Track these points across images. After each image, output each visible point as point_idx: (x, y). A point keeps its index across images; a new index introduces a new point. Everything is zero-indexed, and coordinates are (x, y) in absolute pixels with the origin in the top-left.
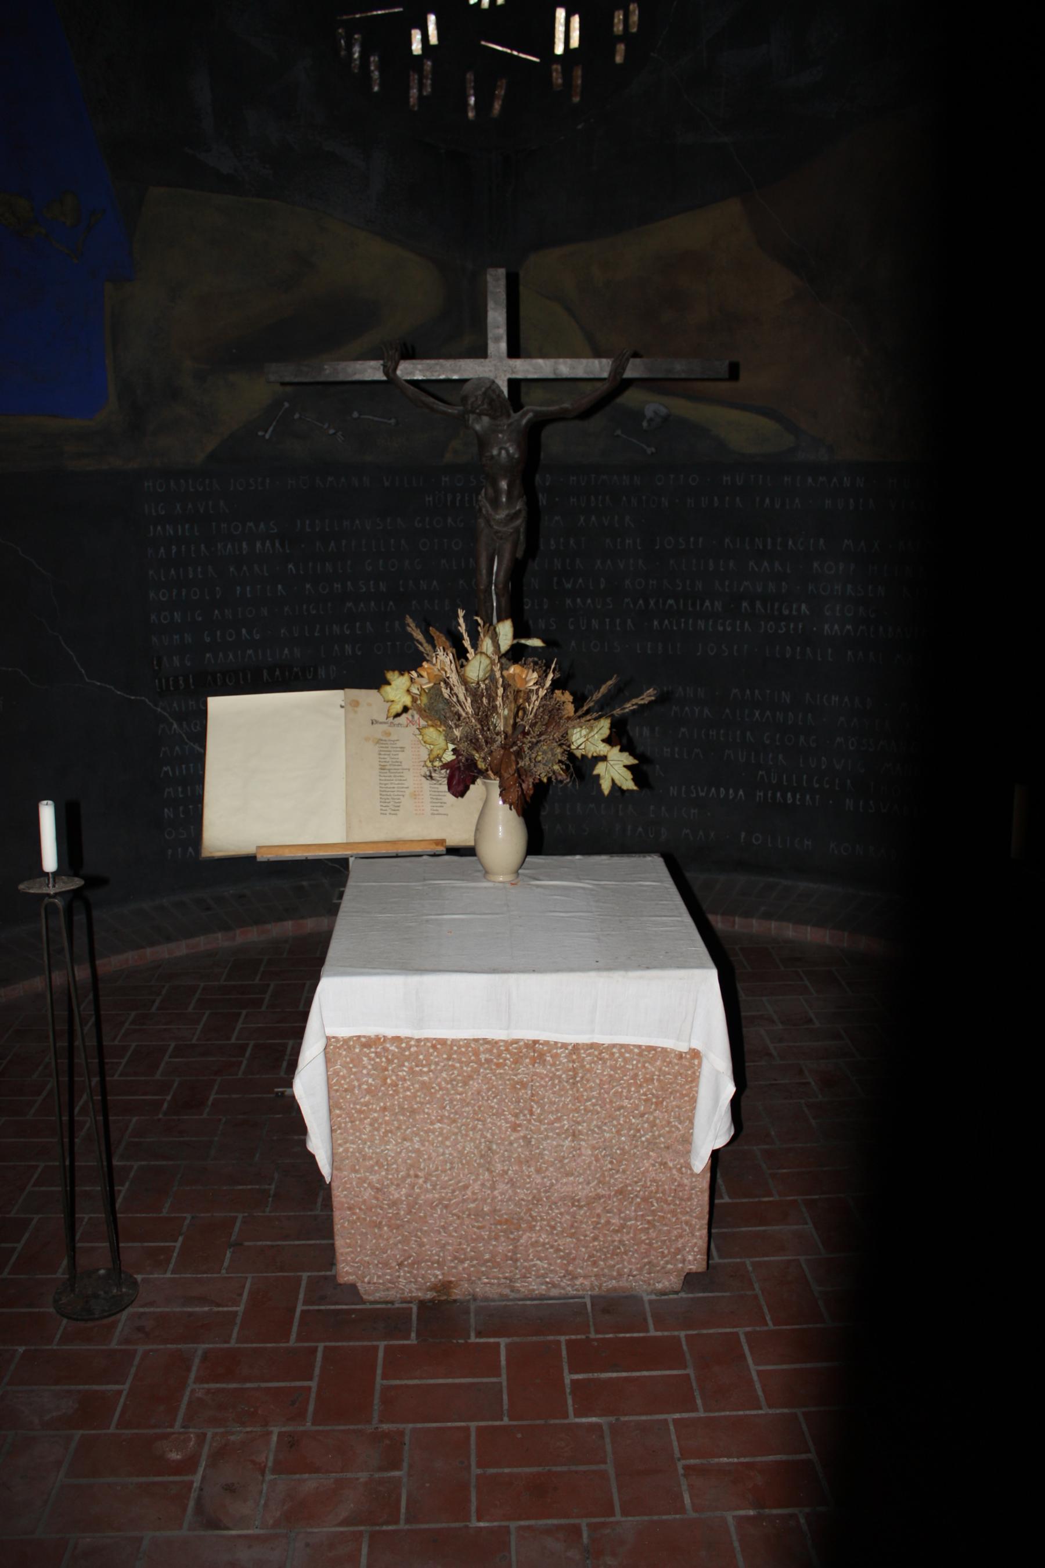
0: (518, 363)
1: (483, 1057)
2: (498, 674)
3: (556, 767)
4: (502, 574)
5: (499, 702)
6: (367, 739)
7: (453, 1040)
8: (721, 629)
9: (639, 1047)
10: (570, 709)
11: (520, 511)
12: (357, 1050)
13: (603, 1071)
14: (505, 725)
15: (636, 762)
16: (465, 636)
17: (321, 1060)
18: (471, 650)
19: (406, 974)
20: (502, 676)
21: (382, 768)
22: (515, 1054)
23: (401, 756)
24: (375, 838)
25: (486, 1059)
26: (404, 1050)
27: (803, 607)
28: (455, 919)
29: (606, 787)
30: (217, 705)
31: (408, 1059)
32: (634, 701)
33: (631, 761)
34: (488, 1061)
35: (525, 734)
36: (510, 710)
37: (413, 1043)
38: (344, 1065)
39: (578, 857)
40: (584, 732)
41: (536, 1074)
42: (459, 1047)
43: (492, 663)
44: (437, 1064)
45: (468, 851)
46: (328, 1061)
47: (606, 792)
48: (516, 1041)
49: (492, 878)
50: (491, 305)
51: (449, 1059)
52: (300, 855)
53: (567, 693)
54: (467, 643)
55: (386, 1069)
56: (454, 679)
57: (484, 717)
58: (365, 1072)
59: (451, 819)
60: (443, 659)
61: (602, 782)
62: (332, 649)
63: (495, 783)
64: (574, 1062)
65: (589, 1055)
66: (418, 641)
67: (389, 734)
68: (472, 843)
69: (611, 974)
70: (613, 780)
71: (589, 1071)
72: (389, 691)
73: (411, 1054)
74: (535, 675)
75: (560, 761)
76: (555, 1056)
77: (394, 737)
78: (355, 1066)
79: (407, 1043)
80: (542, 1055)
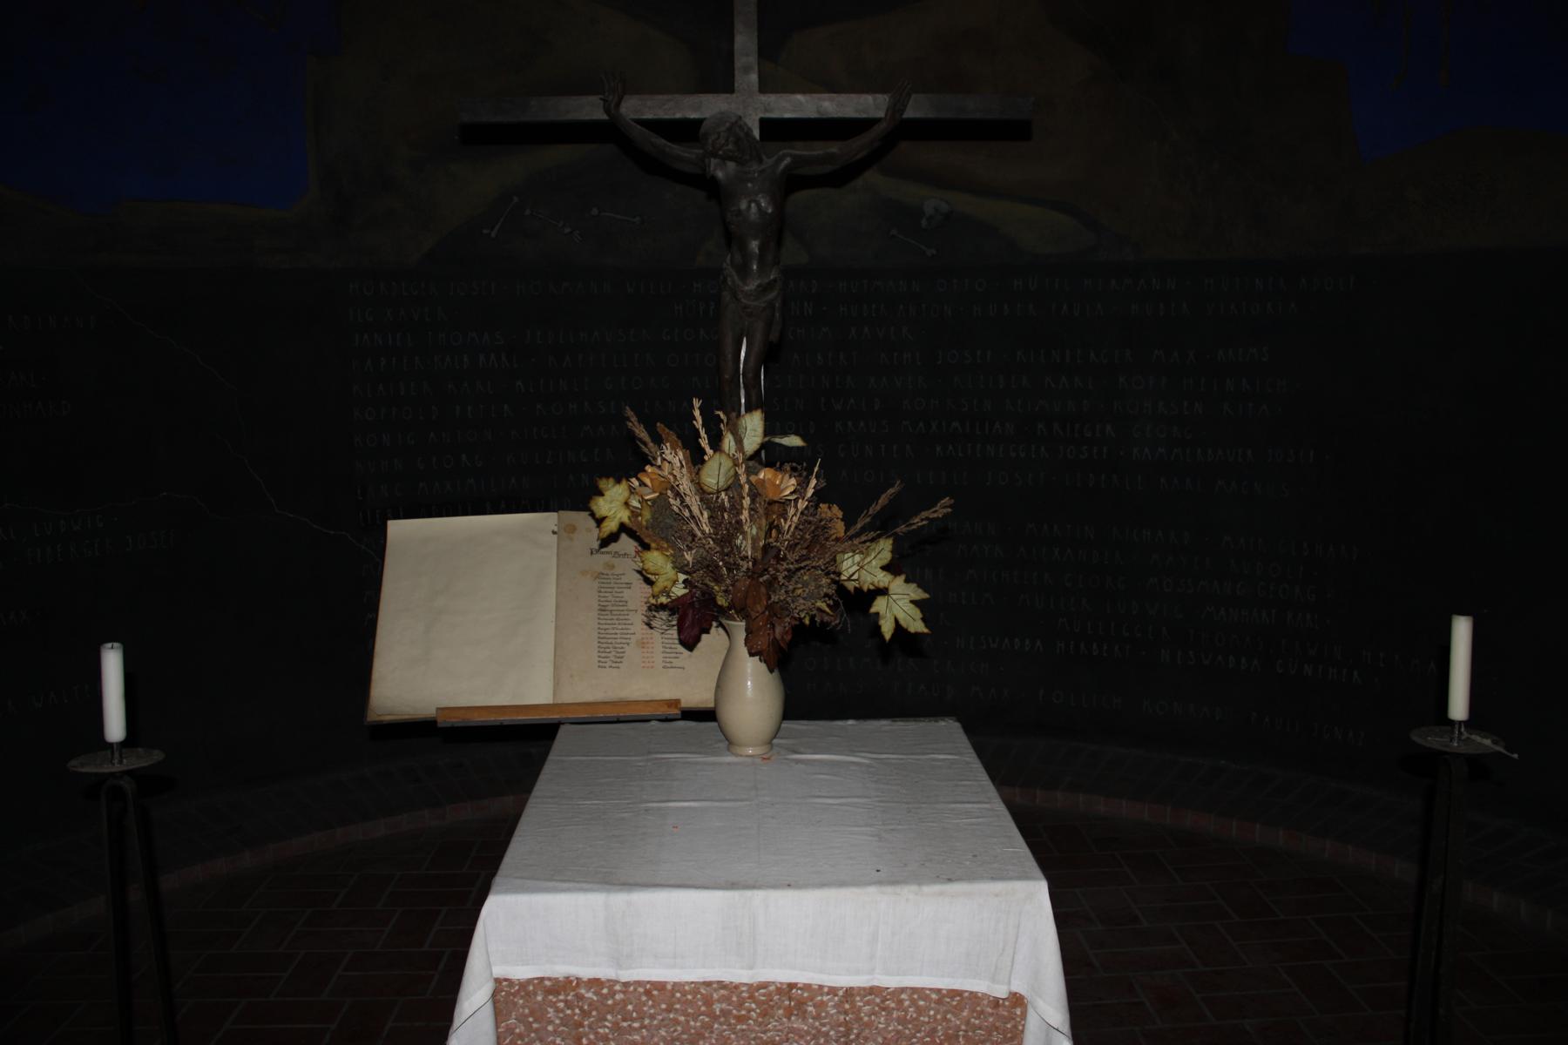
0: (771, 98)
1: (717, 1008)
2: (743, 479)
3: (819, 604)
4: (752, 359)
5: (745, 515)
6: (584, 573)
7: (675, 984)
8: (1013, 455)
9: (938, 991)
10: (840, 527)
11: (775, 280)
12: (539, 998)
13: (888, 1025)
14: (753, 548)
15: (926, 596)
16: (702, 433)
17: (488, 1011)
18: (709, 451)
19: (608, 891)
20: (748, 481)
21: (602, 609)
22: (763, 1002)
23: (626, 594)
24: (589, 697)
25: (722, 1011)
26: (606, 997)
27: (1109, 427)
28: (684, 808)
29: (887, 629)
30: (399, 530)
31: (611, 1010)
32: (924, 514)
33: (919, 594)
34: (724, 1013)
35: (778, 559)
36: (759, 528)
37: (618, 987)
38: (522, 1019)
39: (850, 722)
40: (857, 558)
41: (792, 1030)
42: (684, 994)
43: (736, 464)
44: (652, 1017)
45: (707, 715)
46: (499, 1012)
47: (888, 636)
48: (764, 985)
49: (739, 750)
50: (739, 26)
51: (669, 1010)
52: (492, 719)
53: (835, 508)
54: (704, 443)
55: (581, 1025)
56: (685, 485)
57: (726, 535)
58: (550, 1028)
59: (684, 677)
60: (673, 458)
61: (882, 622)
62: (535, 455)
63: (739, 627)
64: (846, 1013)
65: (867, 1003)
66: (641, 440)
67: (613, 567)
68: (711, 705)
69: (898, 889)
70: (896, 621)
71: (869, 1025)
72: (602, 506)
73: (615, 1004)
74: (793, 481)
75: (826, 595)
76: (821, 1006)
77: (617, 571)
78: (536, 1021)
79: (611, 988)
80: (801, 1004)
